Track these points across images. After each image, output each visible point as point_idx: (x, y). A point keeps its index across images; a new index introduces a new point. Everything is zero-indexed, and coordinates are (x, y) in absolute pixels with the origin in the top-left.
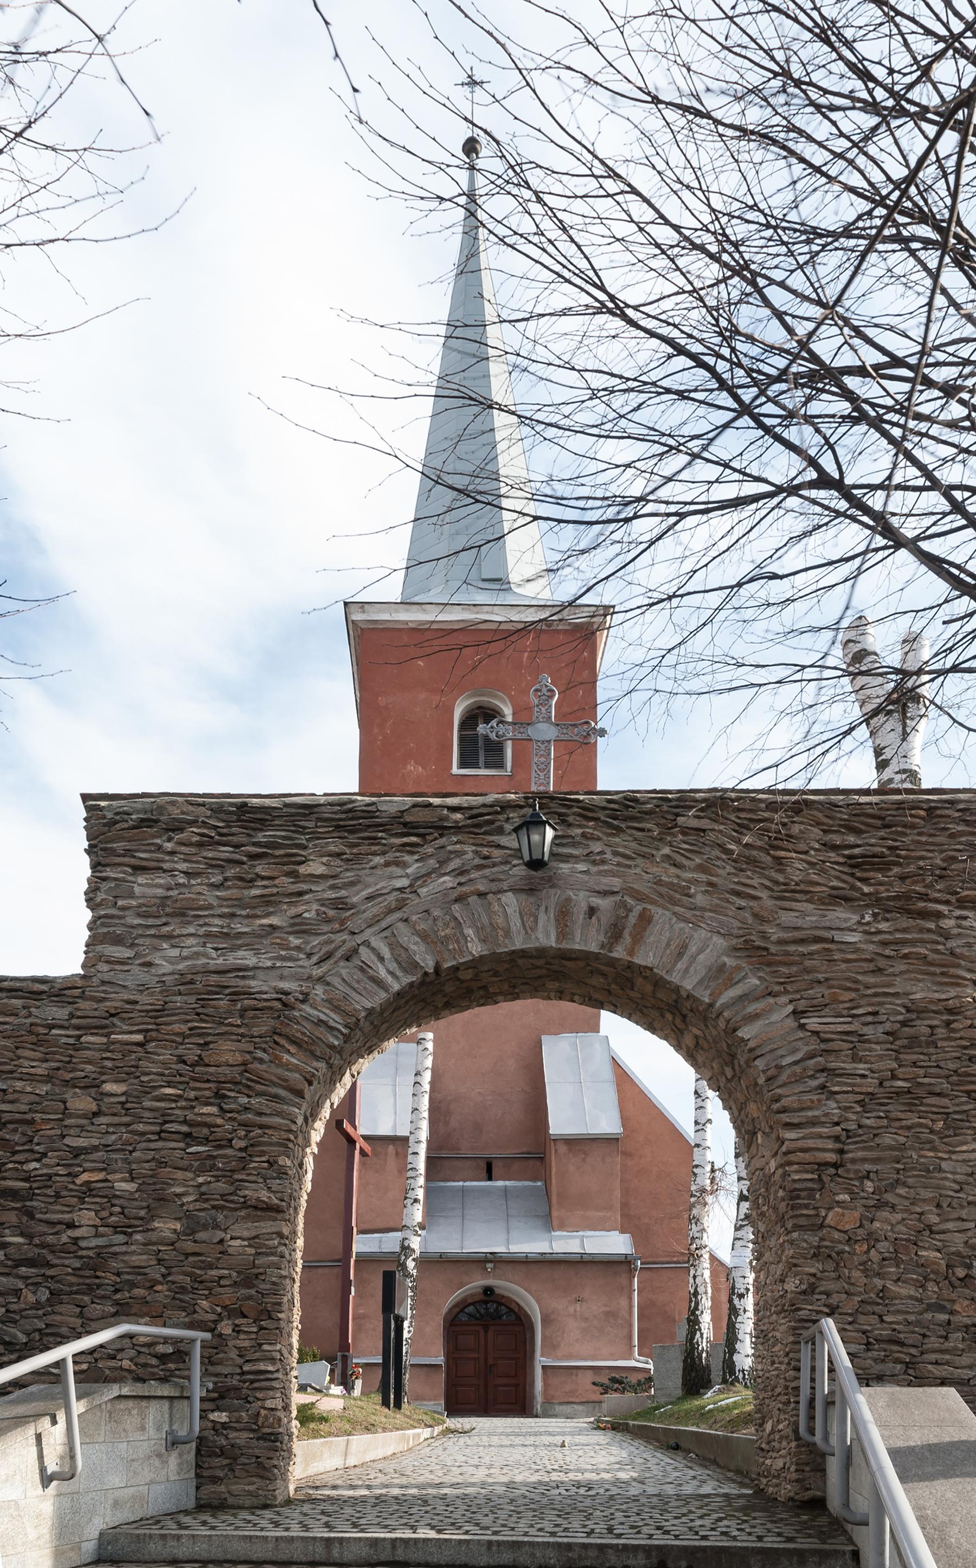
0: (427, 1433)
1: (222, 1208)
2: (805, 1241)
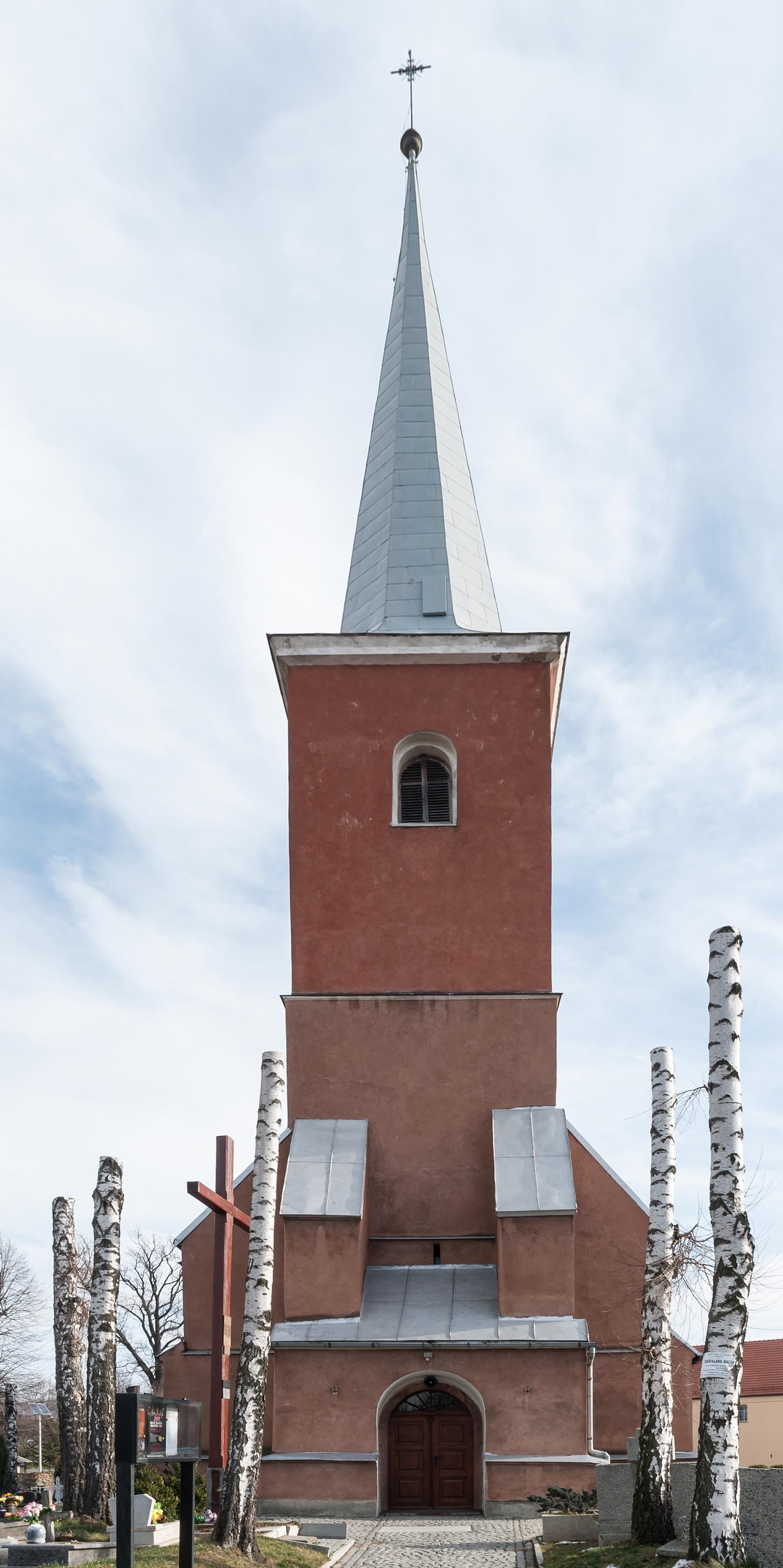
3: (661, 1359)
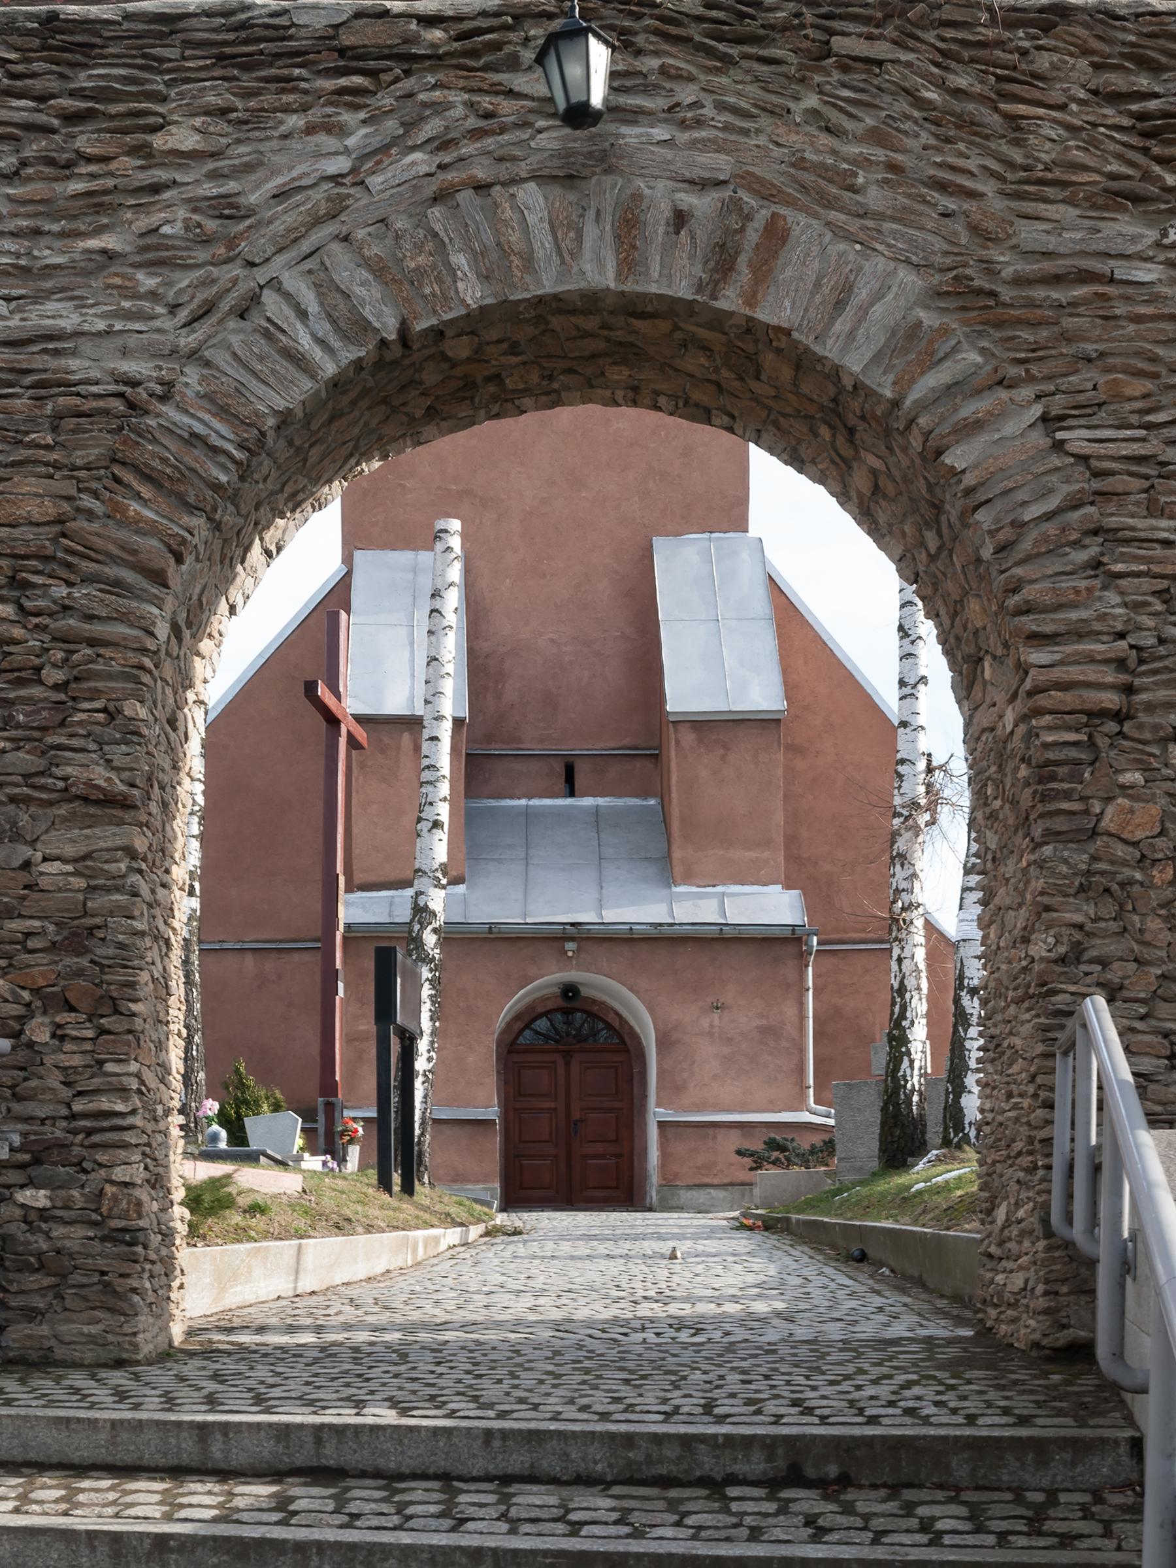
0: (452, 1236)
1: (26, 800)
2: (1065, 861)
3: (912, 929)
